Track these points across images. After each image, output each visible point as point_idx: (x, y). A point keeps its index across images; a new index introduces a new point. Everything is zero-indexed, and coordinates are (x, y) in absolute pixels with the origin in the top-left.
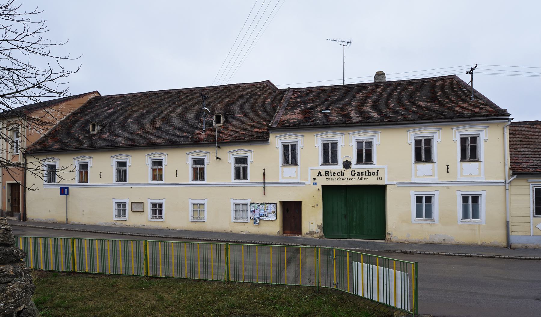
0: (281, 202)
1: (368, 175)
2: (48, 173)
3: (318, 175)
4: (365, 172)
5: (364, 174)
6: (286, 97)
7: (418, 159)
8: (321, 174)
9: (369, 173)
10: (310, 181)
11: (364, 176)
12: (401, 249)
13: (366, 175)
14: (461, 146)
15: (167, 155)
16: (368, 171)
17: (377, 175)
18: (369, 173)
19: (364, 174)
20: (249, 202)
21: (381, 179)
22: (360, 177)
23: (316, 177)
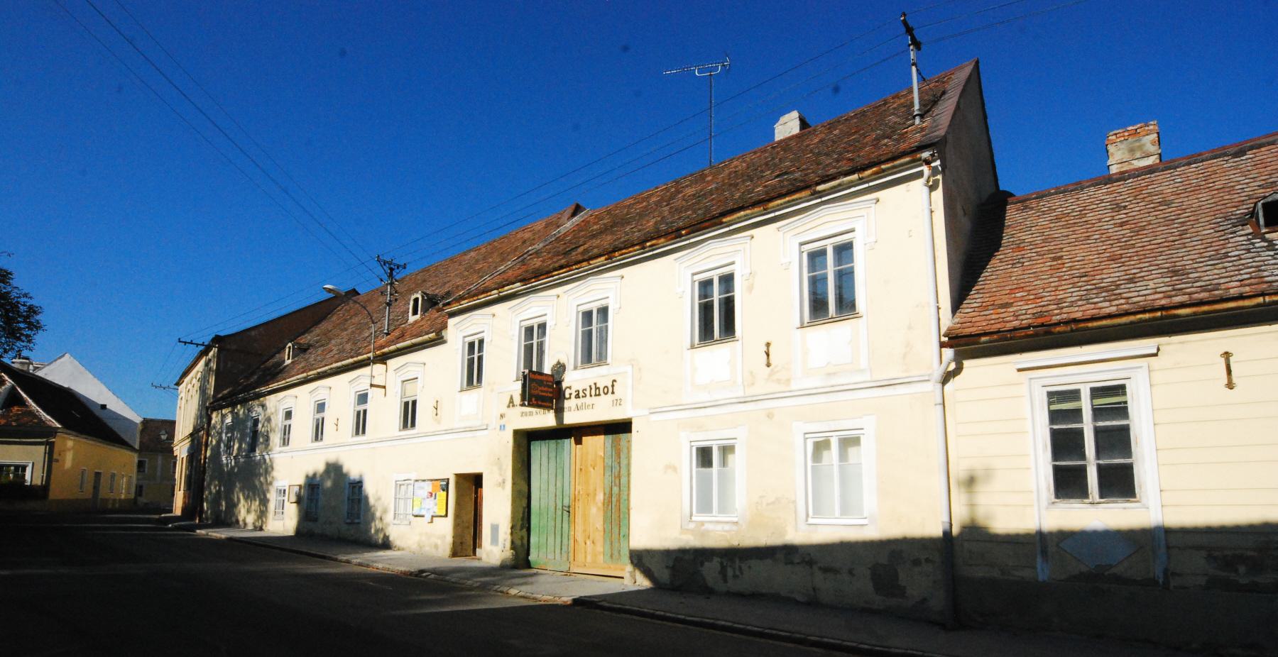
0: (457, 475)
1: (596, 395)
2: (215, 410)
3: (509, 406)
4: (590, 386)
5: (588, 393)
6: (1152, 183)
7: (706, 333)
8: (513, 402)
9: (597, 390)
10: (495, 423)
11: (588, 400)
12: (674, 180)
13: (591, 396)
14: (1054, 434)
15: (113, 476)
16: (595, 384)
17: (613, 393)
18: (597, 390)
19: (588, 393)
20: (414, 477)
21: (620, 405)
22: (579, 401)
23: (504, 409)
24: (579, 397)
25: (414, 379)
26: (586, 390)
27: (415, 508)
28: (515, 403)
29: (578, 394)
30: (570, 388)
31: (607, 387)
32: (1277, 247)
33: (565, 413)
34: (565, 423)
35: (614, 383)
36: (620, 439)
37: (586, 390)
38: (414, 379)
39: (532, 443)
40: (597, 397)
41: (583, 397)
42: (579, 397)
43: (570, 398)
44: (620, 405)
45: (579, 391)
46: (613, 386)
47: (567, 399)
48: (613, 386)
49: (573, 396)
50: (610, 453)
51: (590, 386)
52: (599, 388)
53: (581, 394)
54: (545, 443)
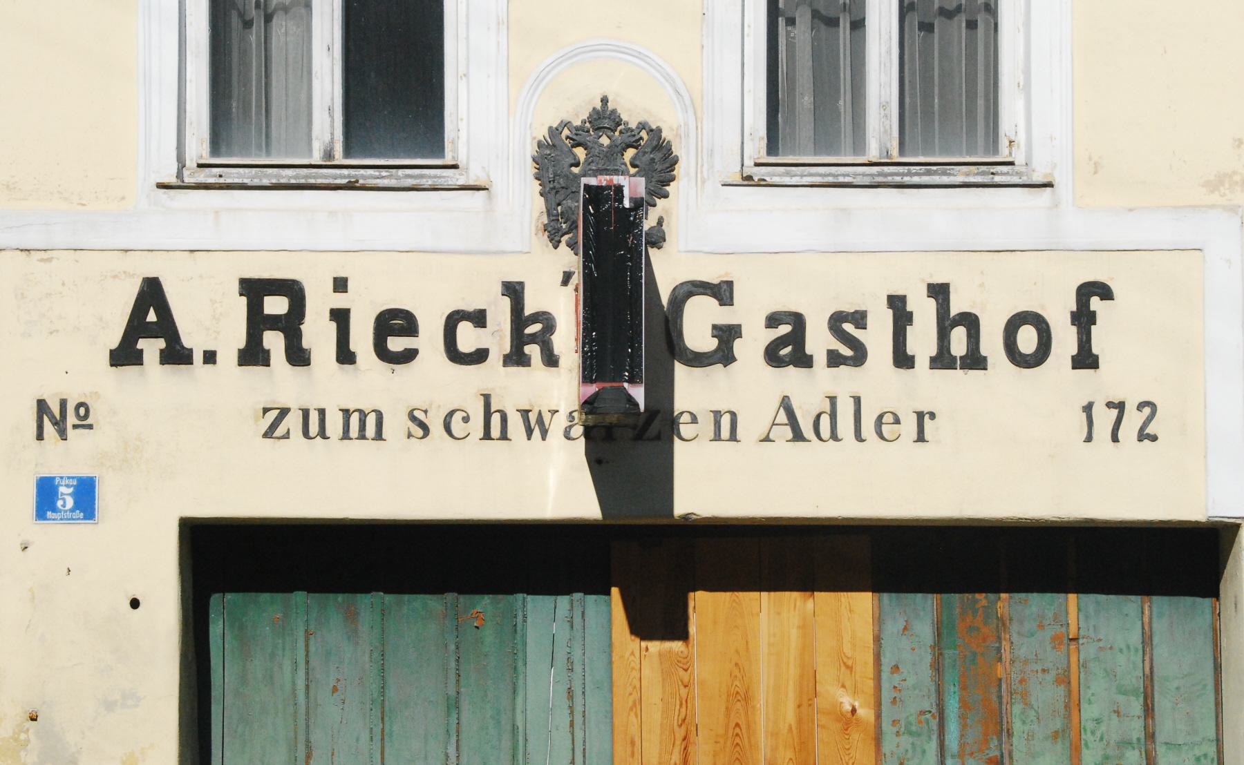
1: (942, 360)
3: (125, 355)
8: (167, 328)
13: (903, 359)
16: (939, 292)
17: (1085, 359)
21: (1143, 436)
24: (803, 360)
25: (498, 45)
26: (859, 319)
27: (1129, 668)
28: (192, 337)
29: (797, 336)
30: (722, 292)
31: (454, 354)
32: (848, 1)
33: (680, 449)
34: (681, 507)
35: (1095, 303)
36: (1002, 624)
37: (859, 319)
38: (498, 45)
39: (215, 599)
40: (957, 376)
41: (835, 359)
42: (803, 360)
43: (724, 356)
44: (1143, 436)
45: (798, 321)
46: (1083, 319)
47: (698, 360)
48: (1083, 319)
49: (751, 347)
50: (929, 704)
51: (897, 304)
52: (970, 322)
53: (819, 341)
54: (351, 616)
